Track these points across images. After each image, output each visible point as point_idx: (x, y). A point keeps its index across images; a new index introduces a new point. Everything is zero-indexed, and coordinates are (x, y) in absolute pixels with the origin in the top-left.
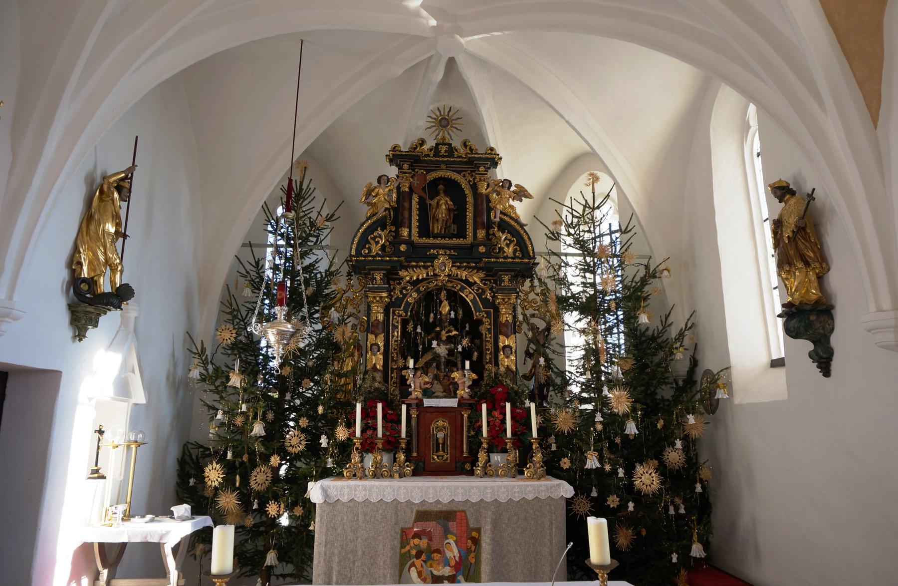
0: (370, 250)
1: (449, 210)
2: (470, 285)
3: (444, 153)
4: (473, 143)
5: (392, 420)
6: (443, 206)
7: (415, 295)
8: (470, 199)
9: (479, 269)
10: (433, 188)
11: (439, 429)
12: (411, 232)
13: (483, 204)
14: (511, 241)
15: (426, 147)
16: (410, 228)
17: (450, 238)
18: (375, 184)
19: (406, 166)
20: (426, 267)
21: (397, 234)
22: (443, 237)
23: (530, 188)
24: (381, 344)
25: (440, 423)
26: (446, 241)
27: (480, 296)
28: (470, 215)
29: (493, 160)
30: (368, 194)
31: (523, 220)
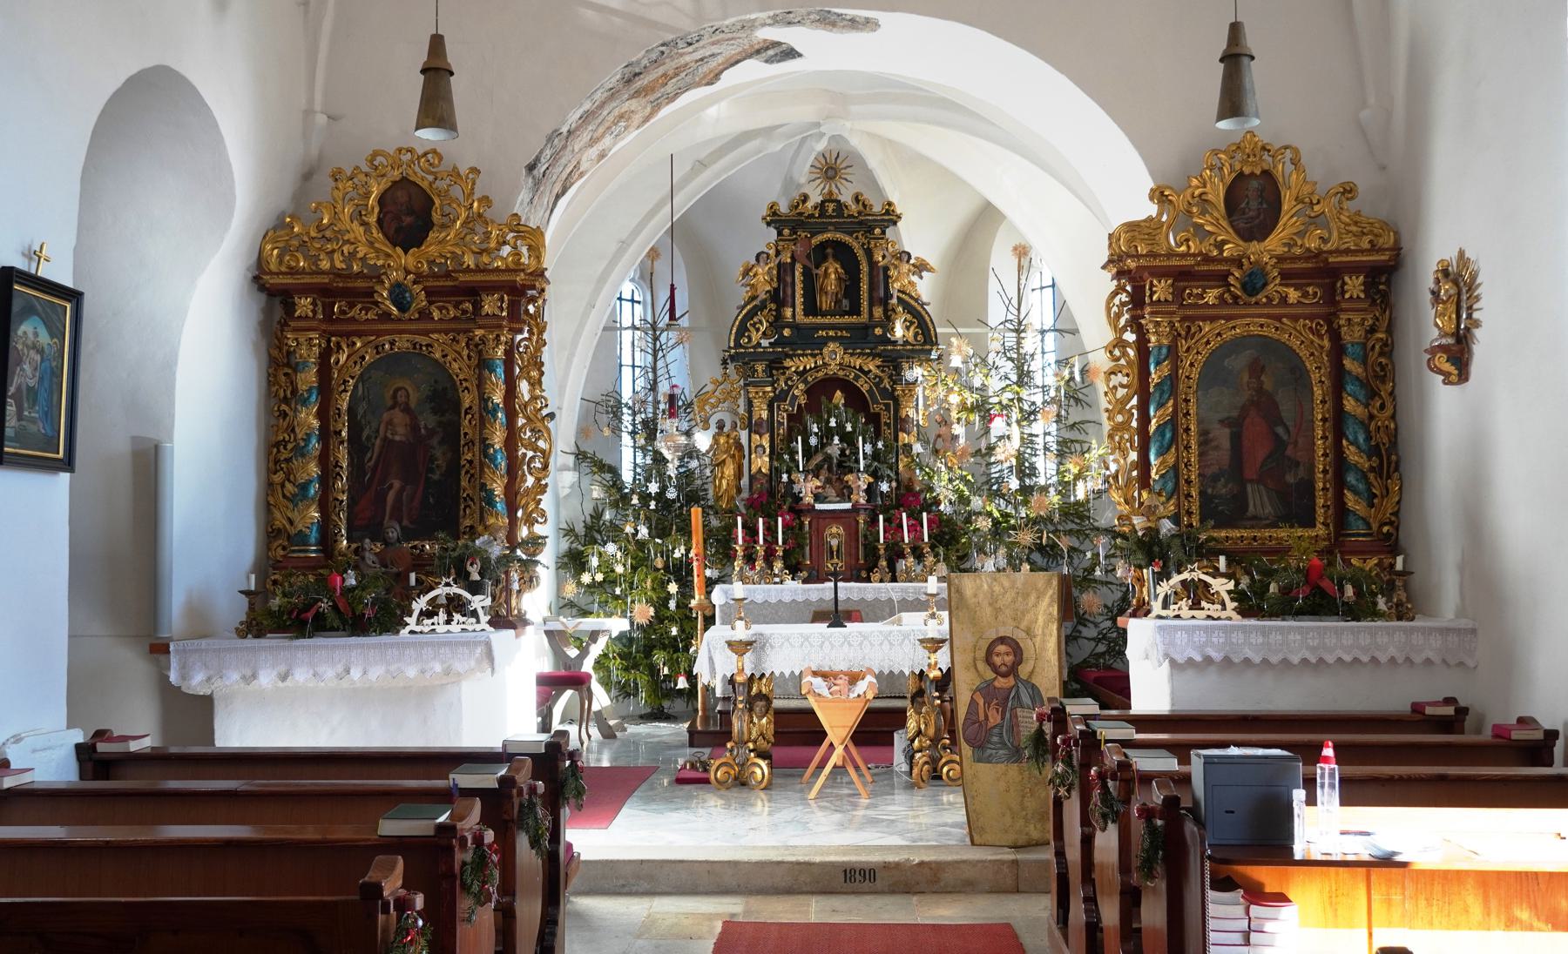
0: (750, 338)
1: (839, 279)
2: (867, 373)
3: (831, 211)
4: (869, 196)
5: (915, 528)
6: (832, 272)
7: (802, 386)
8: (864, 267)
9: (875, 356)
10: (820, 254)
11: (833, 536)
12: (795, 312)
13: (881, 276)
14: (912, 323)
15: (809, 204)
16: (793, 306)
17: (842, 315)
18: (753, 261)
19: (786, 232)
20: (813, 356)
21: (779, 316)
22: (833, 315)
23: (932, 261)
24: (767, 446)
25: (834, 530)
26: (837, 320)
27: (877, 385)
28: (864, 287)
29: (890, 217)
30: (746, 273)
31: (925, 299)
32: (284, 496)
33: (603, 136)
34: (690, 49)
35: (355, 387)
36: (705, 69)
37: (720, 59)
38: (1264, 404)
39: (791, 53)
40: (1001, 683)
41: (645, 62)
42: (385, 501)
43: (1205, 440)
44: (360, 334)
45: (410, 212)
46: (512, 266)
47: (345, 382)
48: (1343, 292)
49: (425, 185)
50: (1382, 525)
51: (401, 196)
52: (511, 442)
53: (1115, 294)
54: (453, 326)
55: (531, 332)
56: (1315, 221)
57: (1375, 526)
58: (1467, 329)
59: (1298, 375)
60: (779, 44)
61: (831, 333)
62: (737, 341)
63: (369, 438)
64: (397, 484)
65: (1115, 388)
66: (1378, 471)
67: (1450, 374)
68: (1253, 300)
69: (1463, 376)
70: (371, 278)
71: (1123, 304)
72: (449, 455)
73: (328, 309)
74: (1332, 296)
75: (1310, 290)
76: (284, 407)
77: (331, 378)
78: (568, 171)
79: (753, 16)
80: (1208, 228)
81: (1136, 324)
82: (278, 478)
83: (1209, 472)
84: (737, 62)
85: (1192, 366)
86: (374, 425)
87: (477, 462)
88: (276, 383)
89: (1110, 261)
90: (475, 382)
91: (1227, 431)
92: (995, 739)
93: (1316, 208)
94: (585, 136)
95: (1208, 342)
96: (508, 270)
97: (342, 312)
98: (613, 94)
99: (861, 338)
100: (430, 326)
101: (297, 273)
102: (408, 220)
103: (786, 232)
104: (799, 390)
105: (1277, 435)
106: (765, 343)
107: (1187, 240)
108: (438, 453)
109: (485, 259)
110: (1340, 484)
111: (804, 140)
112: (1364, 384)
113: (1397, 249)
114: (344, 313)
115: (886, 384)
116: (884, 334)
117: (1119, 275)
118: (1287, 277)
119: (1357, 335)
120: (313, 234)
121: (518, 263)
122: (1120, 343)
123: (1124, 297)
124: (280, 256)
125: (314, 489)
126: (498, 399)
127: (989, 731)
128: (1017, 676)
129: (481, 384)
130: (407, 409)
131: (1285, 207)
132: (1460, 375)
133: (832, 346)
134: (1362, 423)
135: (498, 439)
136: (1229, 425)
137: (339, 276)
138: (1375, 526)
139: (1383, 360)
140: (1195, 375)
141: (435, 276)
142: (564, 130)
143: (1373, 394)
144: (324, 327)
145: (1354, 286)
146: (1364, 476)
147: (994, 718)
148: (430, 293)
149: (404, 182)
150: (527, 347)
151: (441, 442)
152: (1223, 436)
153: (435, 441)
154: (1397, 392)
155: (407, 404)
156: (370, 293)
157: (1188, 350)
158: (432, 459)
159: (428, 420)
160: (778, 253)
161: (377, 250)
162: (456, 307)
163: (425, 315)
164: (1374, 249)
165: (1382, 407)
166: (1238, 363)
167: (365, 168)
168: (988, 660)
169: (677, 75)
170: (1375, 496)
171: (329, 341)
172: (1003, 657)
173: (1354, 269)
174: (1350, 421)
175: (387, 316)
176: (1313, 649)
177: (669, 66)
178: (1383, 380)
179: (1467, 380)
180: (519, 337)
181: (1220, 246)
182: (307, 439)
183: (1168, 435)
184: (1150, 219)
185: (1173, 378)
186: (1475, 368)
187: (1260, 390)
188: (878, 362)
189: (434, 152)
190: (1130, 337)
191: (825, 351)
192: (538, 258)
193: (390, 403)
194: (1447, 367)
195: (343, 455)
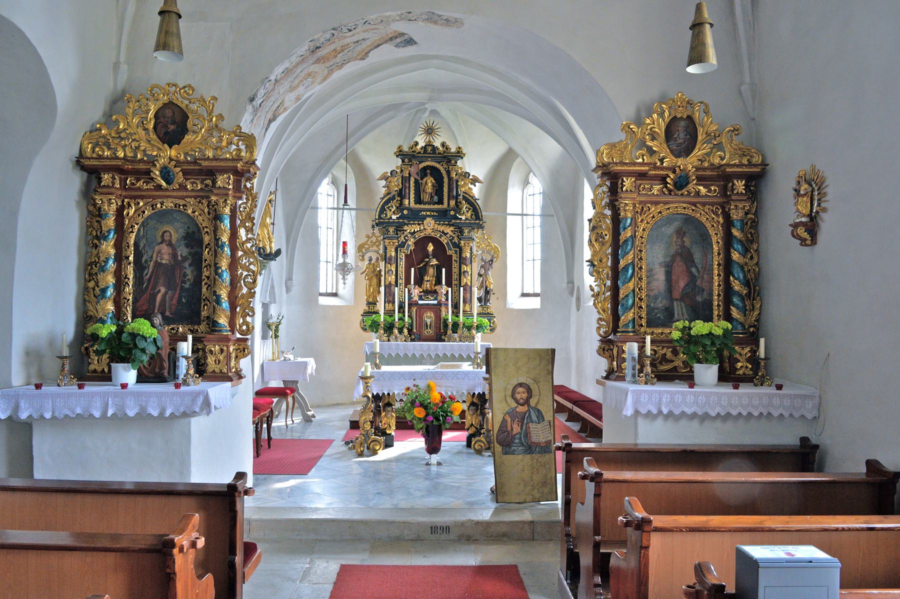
1: (433, 185)
2: (446, 234)
3: (430, 150)
6: (429, 182)
7: (412, 240)
8: (446, 180)
9: (450, 225)
12: (410, 202)
15: (419, 147)
19: (406, 160)
20: (419, 224)
21: (401, 204)
23: (481, 178)
24: (394, 270)
27: (451, 240)
28: (446, 190)
32: (95, 296)
33: (298, 86)
34: (350, 34)
35: (139, 230)
36: (359, 48)
37: (368, 43)
39: (410, 42)
40: (521, 409)
41: (322, 40)
42: (155, 300)
44: (142, 197)
45: (174, 123)
46: (235, 157)
47: (132, 227)
48: (733, 190)
49: (183, 106)
50: (750, 327)
51: (168, 113)
52: (234, 264)
54: (201, 194)
55: (247, 199)
56: (719, 147)
58: (817, 212)
59: (704, 239)
60: (403, 34)
61: (428, 213)
62: (380, 216)
63: (146, 261)
64: (163, 290)
66: (749, 295)
67: (806, 240)
69: (814, 242)
70: (149, 163)
72: (195, 273)
73: (123, 182)
74: (726, 193)
76: (96, 241)
77: (123, 224)
78: (276, 105)
79: (388, 14)
82: (91, 284)
83: (652, 294)
84: (379, 46)
86: (150, 253)
87: (212, 278)
88: (91, 226)
89: (598, 166)
90: (212, 229)
92: (517, 441)
94: (286, 85)
95: (653, 217)
96: (233, 160)
97: (133, 184)
98: (303, 60)
99: (442, 216)
100: (185, 194)
101: (104, 158)
102: (172, 127)
103: (406, 160)
104: (411, 242)
105: (691, 272)
106: (394, 217)
108: (189, 271)
109: (219, 153)
111: (417, 112)
112: (743, 245)
113: (764, 164)
114: (133, 184)
115: (456, 240)
116: (455, 215)
118: (701, 179)
120: (113, 135)
121: (238, 155)
123: (605, 189)
124: (93, 149)
125: (110, 292)
126: (225, 239)
127: (513, 437)
128: (529, 405)
129: (216, 229)
130: (170, 244)
131: (700, 138)
132: (812, 240)
133: (428, 219)
135: (224, 264)
137: (128, 161)
139: (753, 231)
141: (188, 162)
142: (273, 78)
143: (746, 250)
144: (120, 192)
145: (740, 185)
147: (516, 429)
148: (185, 173)
149: (170, 104)
150: (245, 208)
151: (190, 265)
153: (186, 264)
155: (170, 241)
156: (148, 172)
158: (185, 275)
159: (183, 251)
160: (402, 171)
161: (153, 146)
162: (202, 183)
163: (183, 187)
164: (750, 164)
165: (752, 258)
166: (670, 230)
167: (148, 96)
168: (513, 396)
169: (343, 51)
171: (123, 201)
172: (521, 394)
173: (740, 176)
174: (736, 266)
175: (159, 187)
177: (337, 45)
178: (752, 242)
179: (816, 243)
180: (240, 202)
181: (662, 161)
182: (106, 262)
183: (630, 271)
184: (621, 141)
186: (822, 237)
188: (452, 228)
189: (190, 86)
190: (608, 212)
191: (425, 222)
192: (252, 153)
193: (160, 240)
194: (805, 235)
195: (130, 271)
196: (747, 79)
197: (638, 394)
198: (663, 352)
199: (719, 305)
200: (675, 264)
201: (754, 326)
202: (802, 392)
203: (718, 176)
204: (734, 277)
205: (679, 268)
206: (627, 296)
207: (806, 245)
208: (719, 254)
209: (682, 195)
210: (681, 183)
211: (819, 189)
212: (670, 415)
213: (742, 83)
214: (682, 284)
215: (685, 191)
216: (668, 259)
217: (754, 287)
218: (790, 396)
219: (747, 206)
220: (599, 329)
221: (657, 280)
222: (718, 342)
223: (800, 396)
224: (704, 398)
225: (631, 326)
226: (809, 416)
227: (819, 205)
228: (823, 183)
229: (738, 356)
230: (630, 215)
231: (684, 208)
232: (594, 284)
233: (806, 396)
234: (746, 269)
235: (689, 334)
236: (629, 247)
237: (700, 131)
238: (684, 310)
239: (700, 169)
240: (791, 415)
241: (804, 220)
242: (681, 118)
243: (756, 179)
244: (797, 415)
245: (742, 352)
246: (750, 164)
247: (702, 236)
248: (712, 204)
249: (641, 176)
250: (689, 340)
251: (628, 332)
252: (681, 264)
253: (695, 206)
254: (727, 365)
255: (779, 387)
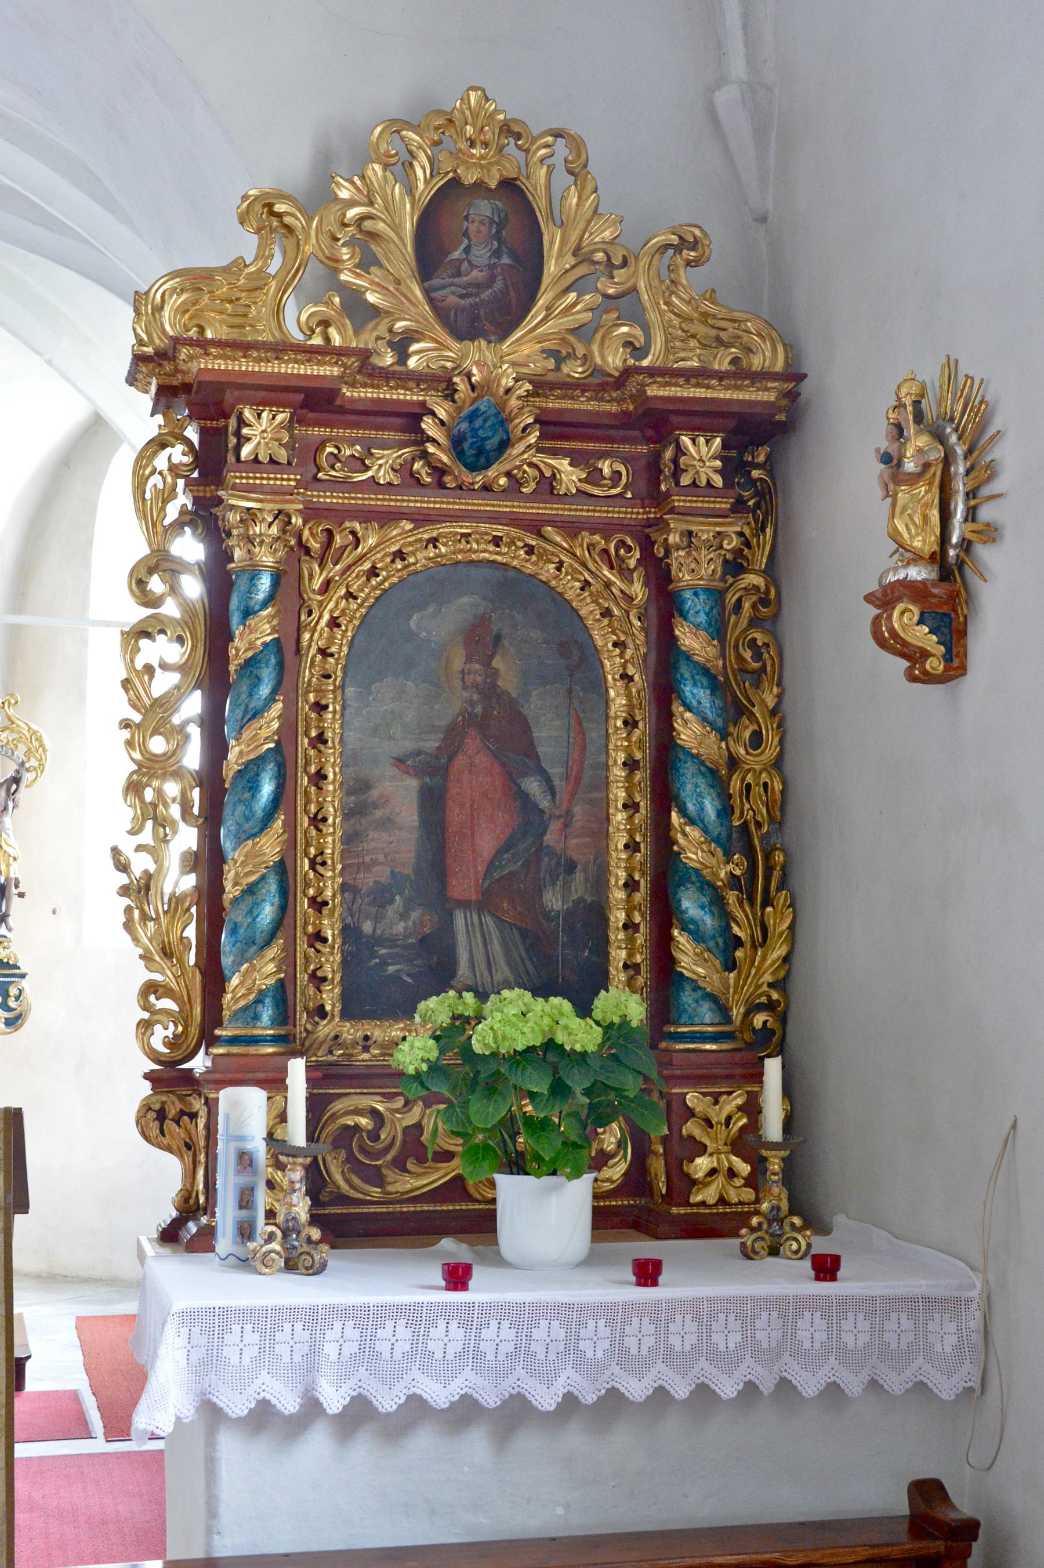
38: (500, 727)
43: (360, 804)
48: (677, 472)
50: (753, 1008)
53: (159, 443)
56: (624, 304)
57: (737, 1013)
58: (966, 545)
59: (576, 663)
65: (149, 669)
66: (743, 884)
67: (925, 654)
68: (479, 479)
69: (955, 666)
71: (174, 469)
74: (654, 482)
75: (606, 467)
80: (371, 298)
81: (205, 517)
83: (367, 881)
85: (331, 620)
91: (413, 783)
93: (620, 275)
95: (373, 572)
105: (524, 799)
107: (325, 323)
110: (664, 915)
112: (716, 685)
117: (167, 396)
118: (555, 429)
119: (706, 570)
122: (159, 562)
123: (177, 454)
131: (551, 268)
132: (948, 657)
134: (713, 773)
136: (418, 772)
138: (737, 1013)
139: (760, 638)
140: (340, 647)
143: (734, 710)
145: (702, 454)
146: (717, 903)
152: (401, 796)
154: (786, 706)
157: (327, 584)
166: (442, 624)
170: (738, 943)
176: (593, 1369)
178: (758, 676)
179: (963, 670)
181: (401, 346)
183: (267, 789)
184: (239, 263)
185: (285, 652)
186: (984, 643)
187: (490, 692)
190: (189, 548)
194: (922, 636)
196: (738, 67)
197: (211, 1323)
198: (411, 1119)
199: (629, 926)
200: (460, 761)
201: (770, 1006)
202: (920, 1286)
203: (625, 422)
204: (683, 812)
205: (476, 773)
206: (251, 890)
207: (928, 678)
208: (630, 723)
209: (486, 488)
210: (479, 444)
211: (970, 451)
212: (359, 1414)
213: (722, 81)
214: (487, 843)
215: (496, 474)
216: (431, 743)
217: (765, 863)
218: (866, 1305)
219: (732, 530)
220: (145, 1027)
221: (387, 823)
222: (578, 1082)
223: (910, 1303)
224: (508, 1334)
225: (267, 1014)
226: (947, 1388)
227: (971, 514)
228: (982, 426)
229: (692, 1128)
230: (267, 559)
231: (497, 541)
232: (127, 845)
233: (930, 1302)
234: (735, 785)
235: (467, 1053)
236: (265, 690)
237: (553, 240)
238: (496, 947)
239: (552, 386)
240: (874, 1385)
241: (916, 573)
242: (479, 186)
243: (763, 437)
244: (896, 1383)
245: (718, 1114)
246: (740, 374)
247: (563, 649)
248: (606, 529)
249: (314, 403)
250: (467, 1073)
251: (255, 1040)
252: (483, 760)
253: (540, 535)
254: (658, 1166)
255: (826, 1268)
